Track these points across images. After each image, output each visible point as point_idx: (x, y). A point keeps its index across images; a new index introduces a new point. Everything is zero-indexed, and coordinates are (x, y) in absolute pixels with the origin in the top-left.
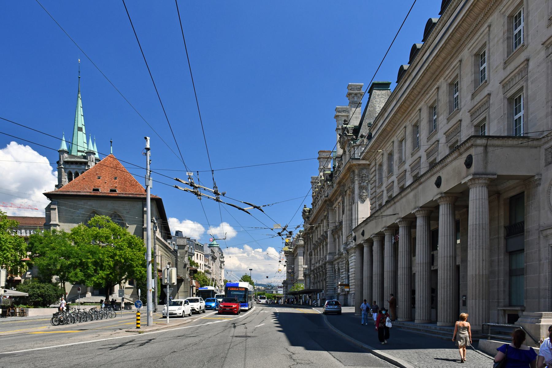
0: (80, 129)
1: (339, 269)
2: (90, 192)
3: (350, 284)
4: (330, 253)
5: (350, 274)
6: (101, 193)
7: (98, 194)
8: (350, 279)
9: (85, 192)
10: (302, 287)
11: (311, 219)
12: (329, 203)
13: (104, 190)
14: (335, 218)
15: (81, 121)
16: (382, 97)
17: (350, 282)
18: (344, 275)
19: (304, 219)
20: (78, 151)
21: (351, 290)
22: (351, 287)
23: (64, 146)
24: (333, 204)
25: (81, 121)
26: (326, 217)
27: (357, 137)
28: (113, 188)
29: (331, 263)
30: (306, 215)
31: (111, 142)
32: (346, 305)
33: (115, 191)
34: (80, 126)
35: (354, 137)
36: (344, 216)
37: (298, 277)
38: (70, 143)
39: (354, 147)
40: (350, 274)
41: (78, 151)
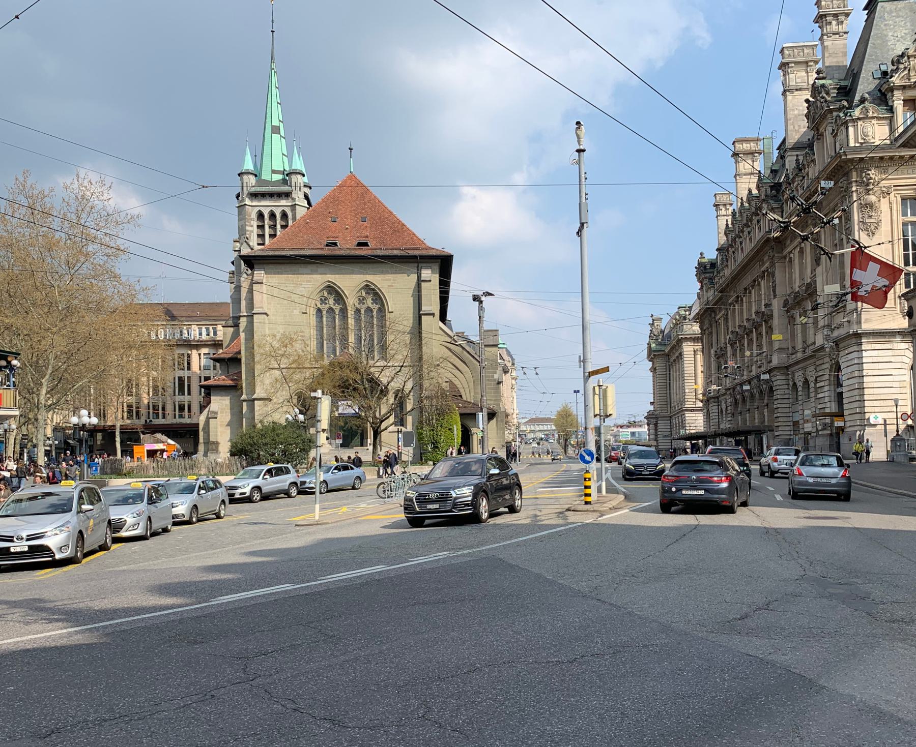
0: (275, 130)
1: (806, 382)
2: (322, 249)
3: (846, 413)
4: (780, 350)
5: (844, 389)
6: (340, 249)
7: (337, 252)
8: (845, 401)
9: (312, 249)
10: (696, 423)
11: (720, 281)
12: (774, 247)
13: (346, 245)
14: (791, 274)
15: (276, 116)
16: (898, 17)
17: (845, 407)
18: (827, 394)
19: (701, 282)
20: (274, 172)
21: (848, 424)
22: (847, 418)
23: (249, 165)
24: (785, 247)
25: (276, 116)
26: (769, 274)
27: (850, 102)
28: (331, 240)
29: (785, 369)
30: (706, 271)
31: (351, 149)
32: (322, 509)
33: (366, 244)
34: (276, 123)
35: (845, 103)
36: (819, 270)
37: (683, 402)
38: (258, 158)
39: (846, 124)
40: (844, 389)
41: (274, 172)
